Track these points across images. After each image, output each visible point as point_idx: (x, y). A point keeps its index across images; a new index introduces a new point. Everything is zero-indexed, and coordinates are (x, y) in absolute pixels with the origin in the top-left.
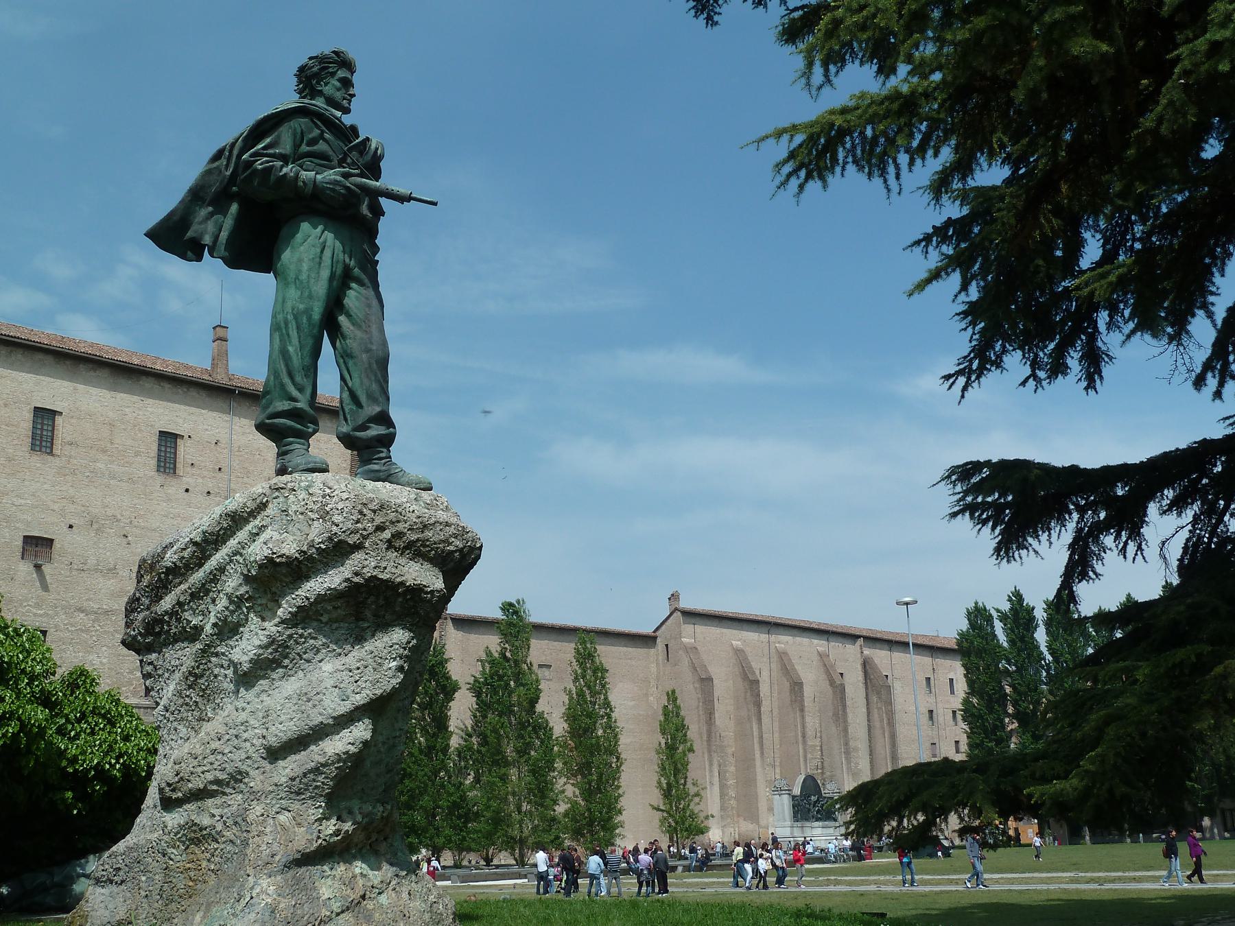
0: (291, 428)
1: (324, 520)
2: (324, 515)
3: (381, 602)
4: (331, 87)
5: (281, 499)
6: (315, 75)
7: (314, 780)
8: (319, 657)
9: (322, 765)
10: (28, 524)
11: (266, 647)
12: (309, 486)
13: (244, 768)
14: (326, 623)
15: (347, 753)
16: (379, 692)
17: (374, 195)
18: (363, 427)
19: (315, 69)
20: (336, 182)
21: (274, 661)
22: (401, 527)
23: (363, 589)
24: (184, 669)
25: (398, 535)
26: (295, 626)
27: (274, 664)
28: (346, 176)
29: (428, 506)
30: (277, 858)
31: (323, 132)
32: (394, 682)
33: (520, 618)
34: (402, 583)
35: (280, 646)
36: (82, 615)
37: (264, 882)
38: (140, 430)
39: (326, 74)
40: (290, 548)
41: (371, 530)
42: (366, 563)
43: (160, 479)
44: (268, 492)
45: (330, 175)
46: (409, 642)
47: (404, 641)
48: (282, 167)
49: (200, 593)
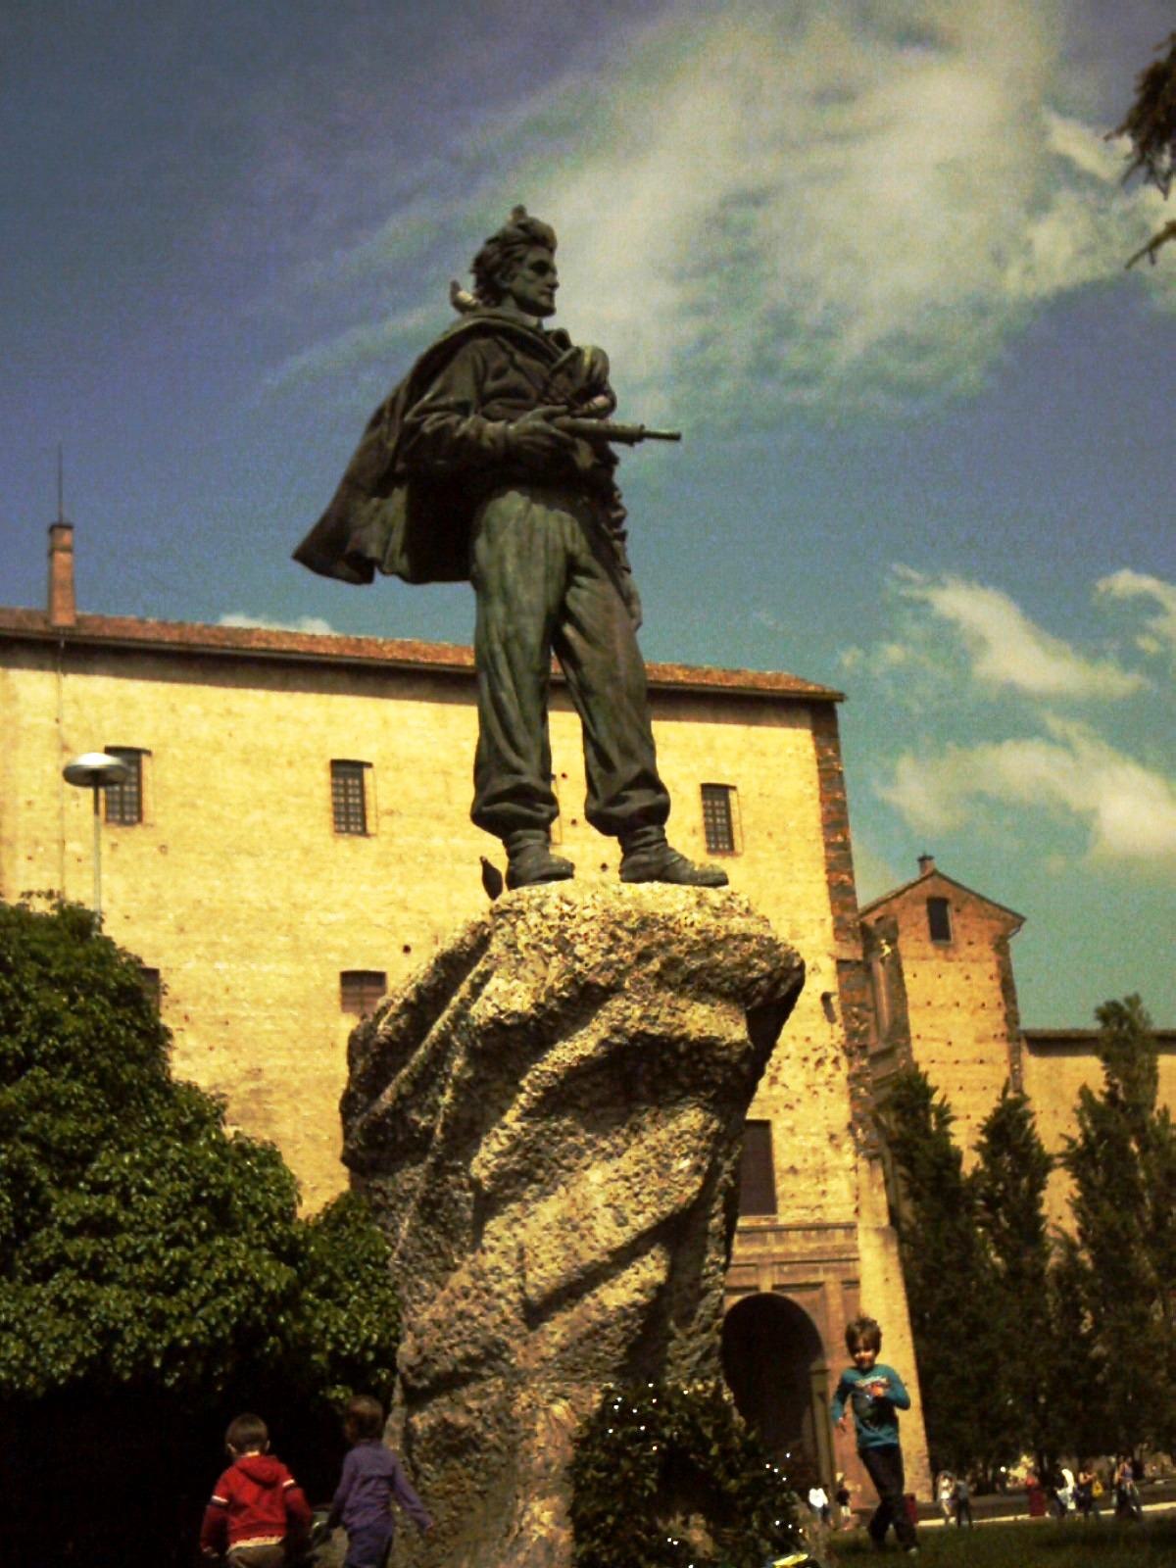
1: (565, 956)
2: (564, 946)
3: (658, 1070)
4: (523, 281)
5: (507, 929)
6: (497, 267)
7: (596, 1350)
8: (584, 1161)
9: (604, 1326)
10: (344, 952)
12: (541, 905)
15: (634, 1305)
16: (667, 1208)
17: (601, 440)
20: (535, 431)
21: (518, 1175)
22: (675, 949)
24: (418, 1195)
25: (672, 964)
26: (546, 1116)
27: (525, 1176)
28: (549, 417)
29: (718, 912)
30: (553, 1469)
31: (511, 355)
32: (689, 1191)
33: (1133, 1030)
34: (684, 1038)
35: (528, 1150)
37: (536, 1507)
41: (630, 961)
44: (488, 919)
45: (530, 420)
46: (705, 1128)
47: (697, 1126)
48: (459, 423)
49: (426, 1080)
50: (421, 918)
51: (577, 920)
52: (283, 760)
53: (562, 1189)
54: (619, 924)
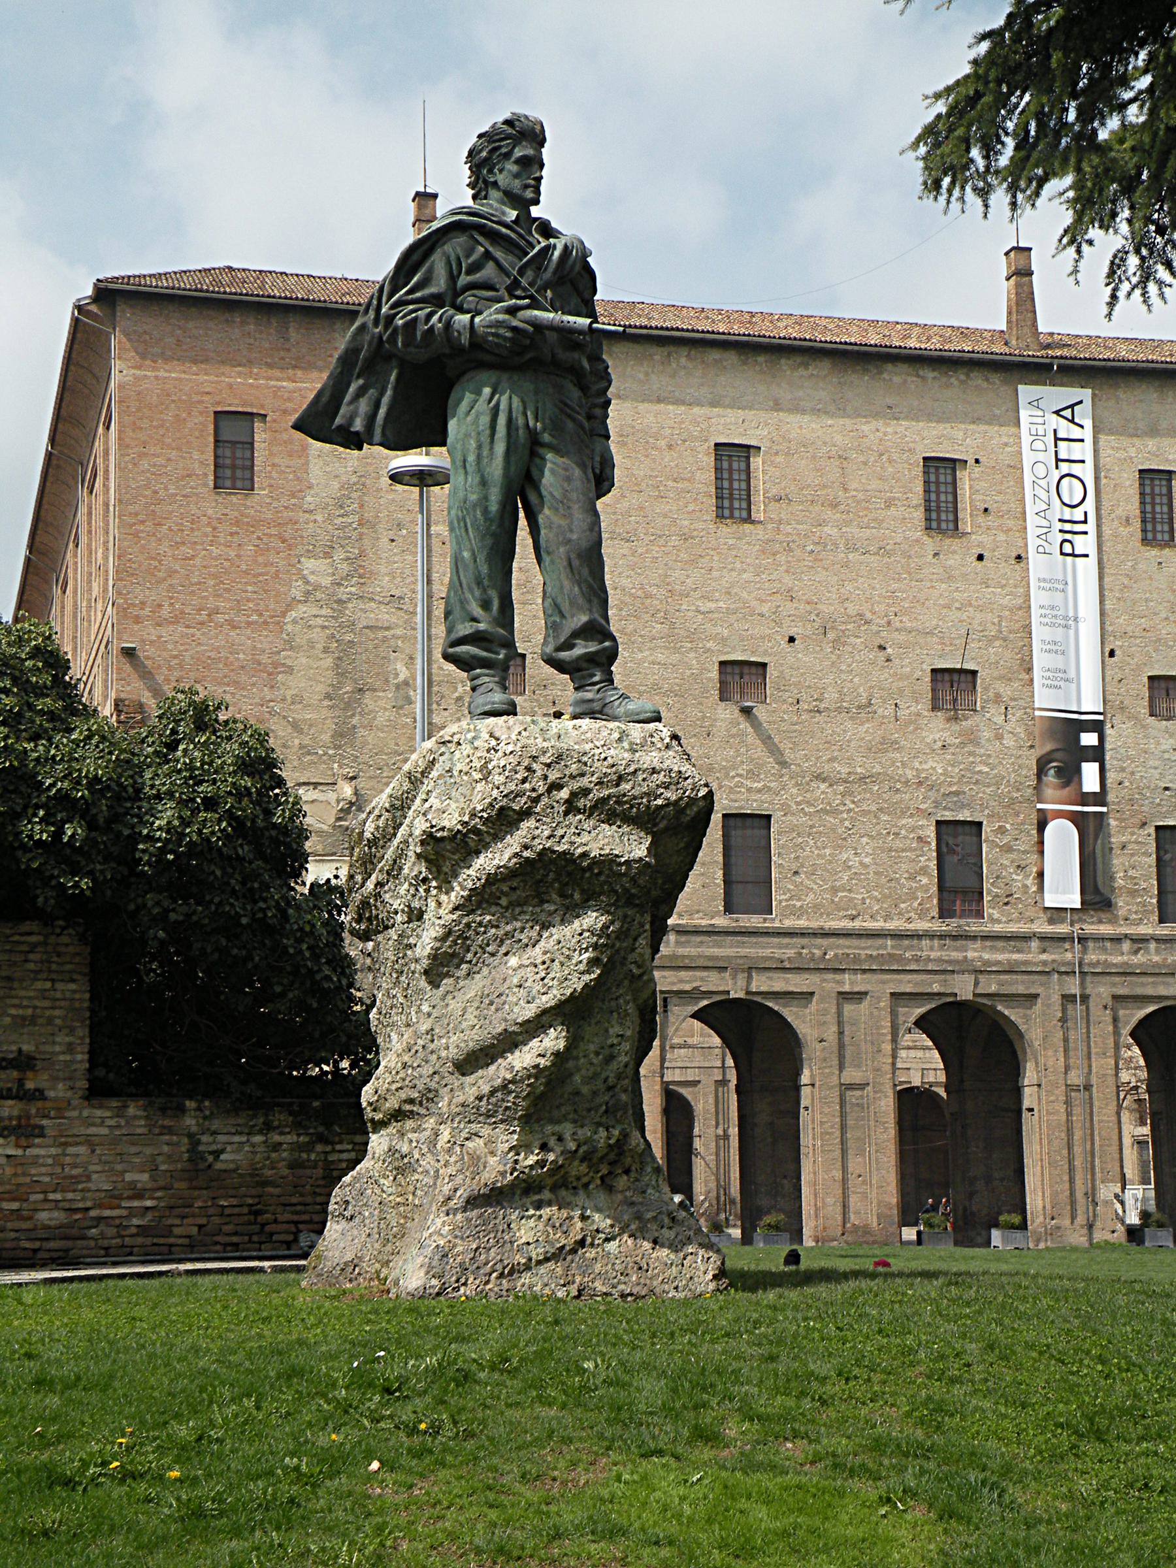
0: (474, 657)
8: (503, 950)
10: (724, 640)
11: (443, 939)
13: (433, 1085)
14: (507, 908)
15: (536, 1066)
18: (568, 645)
19: (484, 154)
20: (498, 324)
22: (584, 782)
23: (539, 865)
26: (472, 912)
28: (512, 311)
30: (459, 1193)
36: (823, 786)
38: (890, 461)
39: (508, 154)
40: (451, 820)
42: (537, 832)
43: (930, 544)
45: (492, 314)
50: (808, 608)
51: (500, 754)
52: (662, 443)
53: (485, 970)
54: (534, 758)
